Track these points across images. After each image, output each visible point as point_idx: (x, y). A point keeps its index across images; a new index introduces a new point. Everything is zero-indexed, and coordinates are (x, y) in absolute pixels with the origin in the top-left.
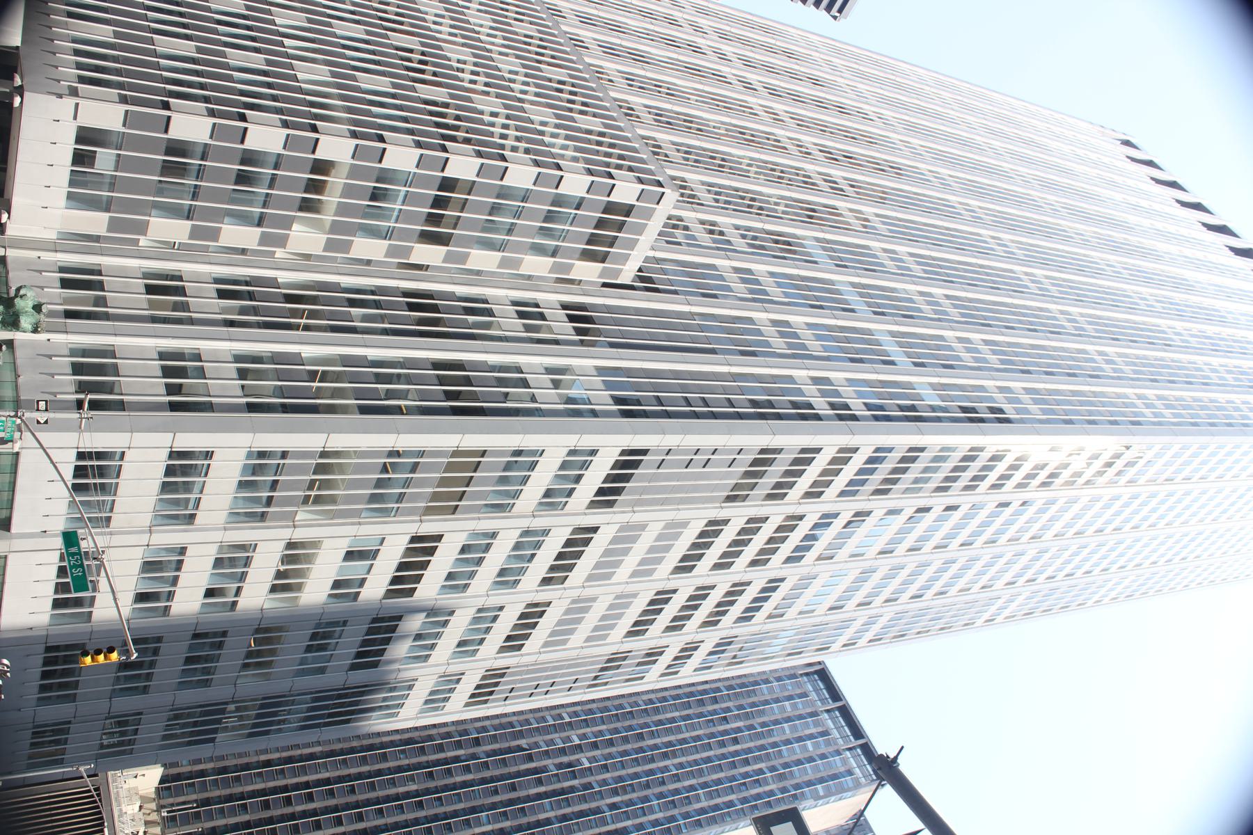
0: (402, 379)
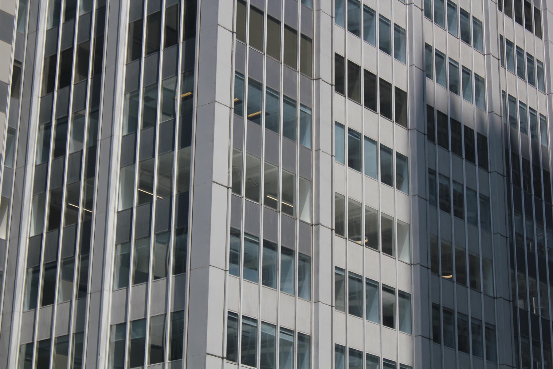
0: (151, 95)
